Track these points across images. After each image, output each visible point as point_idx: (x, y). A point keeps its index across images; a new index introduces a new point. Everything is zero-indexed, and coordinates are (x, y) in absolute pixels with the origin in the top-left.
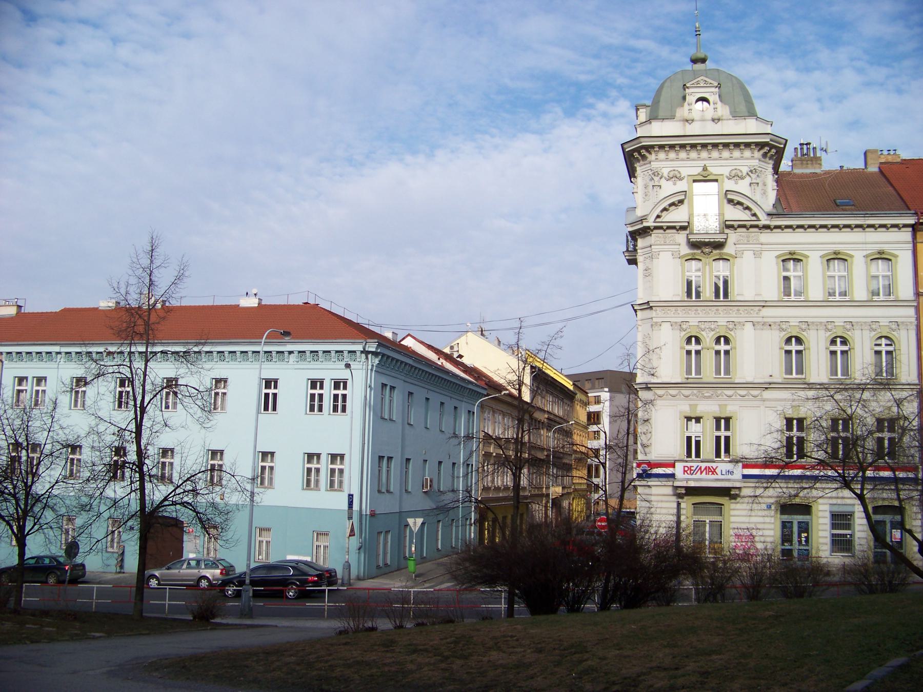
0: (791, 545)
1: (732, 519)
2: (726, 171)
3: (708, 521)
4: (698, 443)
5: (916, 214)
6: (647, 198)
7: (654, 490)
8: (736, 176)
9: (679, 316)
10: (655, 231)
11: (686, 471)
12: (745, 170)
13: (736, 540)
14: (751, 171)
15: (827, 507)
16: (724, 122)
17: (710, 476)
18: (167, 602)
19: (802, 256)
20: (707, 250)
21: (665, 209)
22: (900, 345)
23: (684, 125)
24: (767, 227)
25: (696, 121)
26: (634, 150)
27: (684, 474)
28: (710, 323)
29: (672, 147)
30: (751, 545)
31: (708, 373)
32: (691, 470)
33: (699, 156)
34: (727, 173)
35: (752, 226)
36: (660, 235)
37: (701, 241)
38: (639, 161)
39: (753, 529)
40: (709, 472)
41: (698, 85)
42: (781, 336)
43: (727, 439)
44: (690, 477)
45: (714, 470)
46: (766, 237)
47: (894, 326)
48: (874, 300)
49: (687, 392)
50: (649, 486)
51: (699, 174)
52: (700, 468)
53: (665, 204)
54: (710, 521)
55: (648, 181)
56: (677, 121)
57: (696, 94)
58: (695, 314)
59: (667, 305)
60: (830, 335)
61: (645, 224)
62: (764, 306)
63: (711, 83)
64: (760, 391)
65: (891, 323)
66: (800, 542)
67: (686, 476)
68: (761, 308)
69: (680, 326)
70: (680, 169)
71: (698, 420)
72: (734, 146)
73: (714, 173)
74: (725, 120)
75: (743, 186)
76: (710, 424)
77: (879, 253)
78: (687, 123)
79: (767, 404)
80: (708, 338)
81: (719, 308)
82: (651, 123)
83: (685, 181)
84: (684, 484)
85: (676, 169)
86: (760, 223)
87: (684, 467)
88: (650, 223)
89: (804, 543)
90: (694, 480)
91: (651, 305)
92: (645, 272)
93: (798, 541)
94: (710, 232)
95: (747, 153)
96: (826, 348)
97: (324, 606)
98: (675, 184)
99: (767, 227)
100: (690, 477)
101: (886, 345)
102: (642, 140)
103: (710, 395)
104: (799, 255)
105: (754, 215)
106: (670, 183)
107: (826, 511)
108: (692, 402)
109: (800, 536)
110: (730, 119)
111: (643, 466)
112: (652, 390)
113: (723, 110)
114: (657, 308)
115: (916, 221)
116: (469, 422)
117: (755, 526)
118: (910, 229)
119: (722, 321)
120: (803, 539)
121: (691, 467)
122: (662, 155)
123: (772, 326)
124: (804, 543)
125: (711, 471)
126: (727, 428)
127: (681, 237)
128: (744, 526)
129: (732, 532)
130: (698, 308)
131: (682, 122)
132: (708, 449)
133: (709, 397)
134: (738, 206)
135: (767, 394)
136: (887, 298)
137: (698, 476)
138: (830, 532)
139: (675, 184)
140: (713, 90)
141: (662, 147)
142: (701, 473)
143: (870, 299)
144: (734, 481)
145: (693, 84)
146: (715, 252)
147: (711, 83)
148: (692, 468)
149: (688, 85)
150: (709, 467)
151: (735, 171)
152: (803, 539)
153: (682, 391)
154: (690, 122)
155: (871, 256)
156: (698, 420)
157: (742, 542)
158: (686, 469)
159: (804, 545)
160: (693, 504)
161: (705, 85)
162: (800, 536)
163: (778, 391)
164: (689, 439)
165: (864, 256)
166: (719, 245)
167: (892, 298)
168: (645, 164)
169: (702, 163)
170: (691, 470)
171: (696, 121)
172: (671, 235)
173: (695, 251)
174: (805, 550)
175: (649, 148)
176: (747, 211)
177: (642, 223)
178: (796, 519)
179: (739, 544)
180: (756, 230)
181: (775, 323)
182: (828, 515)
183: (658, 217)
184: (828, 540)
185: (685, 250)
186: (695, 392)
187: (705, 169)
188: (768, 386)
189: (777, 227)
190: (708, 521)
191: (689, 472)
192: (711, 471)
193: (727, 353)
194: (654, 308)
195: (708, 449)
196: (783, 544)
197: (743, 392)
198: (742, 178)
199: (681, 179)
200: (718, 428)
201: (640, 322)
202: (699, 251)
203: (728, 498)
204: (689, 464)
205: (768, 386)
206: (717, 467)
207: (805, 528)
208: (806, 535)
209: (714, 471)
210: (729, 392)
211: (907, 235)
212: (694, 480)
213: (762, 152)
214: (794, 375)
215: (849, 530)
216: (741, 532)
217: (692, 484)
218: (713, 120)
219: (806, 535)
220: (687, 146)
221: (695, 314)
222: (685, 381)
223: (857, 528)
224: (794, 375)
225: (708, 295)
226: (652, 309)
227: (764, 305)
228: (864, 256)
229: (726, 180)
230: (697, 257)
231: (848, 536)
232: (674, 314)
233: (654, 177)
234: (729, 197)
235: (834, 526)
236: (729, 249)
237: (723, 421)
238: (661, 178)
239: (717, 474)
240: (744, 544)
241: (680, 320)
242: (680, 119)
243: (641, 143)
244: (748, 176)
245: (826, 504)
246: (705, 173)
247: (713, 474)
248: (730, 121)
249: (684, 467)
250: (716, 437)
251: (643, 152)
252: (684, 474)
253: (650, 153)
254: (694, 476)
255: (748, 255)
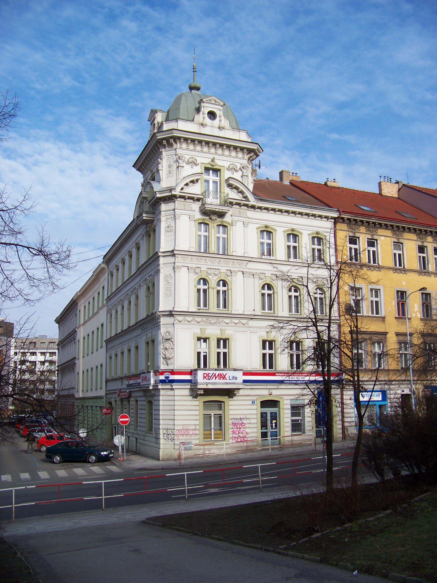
0: (267, 429)
1: (231, 412)
2: (226, 164)
3: (213, 414)
4: (205, 357)
5: (338, 211)
6: (170, 175)
7: (177, 392)
8: (233, 169)
9: (193, 263)
10: (178, 199)
11: (205, 377)
12: (239, 166)
13: (234, 427)
14: (243, 167)
15: (288, 402)
16: (226, 131)
17: (222, 381)
18: (187, 488)
19: (272, 229)
20: (214, 217)
21: (187, 185)
22: (231, 286)
23: (200, 128)
24: (253, 207)
25: (226, 129)
26: (163, 139)
27: (204, 379)
28: (214, 270)
29: (193, 141)
30: (243, 430)
31: (213, 307)
32: (208, 376)
33: (209, 151)
34: (227, 166)
35: (244, 205)
36: (181, 203)
37: (213, 210)
38: (164, 147)
39: (244, 419)
40: (221, 377)
41: (210, 102)
42: (260, 283)
43: (225, 354)
44: (208, 381)
45: (225, 376)
46: (251, 213)
47: (229, 273)
48: (263, 258)
49: (199, 319)
50: (172, 389)
51: (209, 163)
52: (215, 375)
53: (188, 181)
54: (214, 414)
55: (172, 162)
56: (195, 124)
57: (208, 108)
58: (204, 262)
59: (187, 254)
60: (262, 283)
61: (173, 193)
62: (250, 261)
63: (219, 103)
64: (247, 321)
65: (208, 269)
66: (272, 426)
67: (206, 381)
68: (248, 262)
69: (195, 270)
70: (196, 158)
71: (205, 340)
72: (191, 141)
73: (219, 164)
74: (226, 129)
75: (238, 175)
76: (214, 343)
77: (292, 230)
78: (201, 127)
79: (252, 330)
80: (213, 281)
81: (221, 259)
82: (177, 121)
83: (199, 166)
84: (205, 387)
85: (194, 157)
86: (250, 203)
87: (204, 374)
88: (177, 192)
89: (274, 427)
90: (212, 384)
91: (175, 253)
92: (167, 228)
93: (271, 426)
94: (213, 203)
95: (240, 155)
96: (259, 291)
97: (187, 487)
98: (192, 168)
99: (253, 207)
100: (208, 381)
101: (320, 294)
102: (174, 131)
103: (214, 322)
104: (271, 229)
105: (246, 197)
106: (189, 166)
107: (288, 404)
108: (202, 327)
109: (271, 423)
110: (230, 130)
111: (166, 373)
112: (174, 316)
113: (225, 123)
114: (179, 256)
115: (338, 216)
116: (114, 339)
117: (246, 416)
118: (333, 221)
119: (223, 269)
120: (274, 424)
121: (208, 374)
122: (184, 146)
123: (255, 276)
124: (274, 427)
125: (222, 377)
126: (271, 348)
127: (196, 206)
128: (238, 417)
129: (230, 422)
130: (207, 258)
131: (198, 125)
132: (213, 362)
133: (214, 323)
134: (234, 190)
135: (252, 323)
136: (295, 260)
137: (213, 380)
138: (291, 418)
139: (192, 168)
140: (219, 107)
141: (186, 139)
142: (216, 378)
143: (287, 260)
144: (238, 384)
145: (207, 100)
146: (218, 220)
147: (219, 103)
148: (209, 375)
149: (204, 100)
150: (221, 374)
151: (233, 165)
152: (274, 424)
153: (196, 318)
154: (221, 129)
155: (288, 231)
156: (205, 340)
157: (237, 428)
158: (205, 375)
159: (274, 429)
160: (204, 402)
161: (215, 103)
162: (271, 423)
163: (258, 321)
164: (199, 354)
165: (308, 234)
166: (221, 215)
167: (272, 258)
168: (170, 150)
169: (212, 157)
170: (208, 376)
171: (208, 126)
172: (189, 203)
173: (205, 217)
174: (275, 432)
175: (177, 139)
176: (240, 194)
177: (171, 192)
178: (268, 410)
179: (235, 430)
180: (245, 208)
181: (256, 273)
182: (289, 407)
183: (182, 189)
184: (289, 424)
185: (198, 216)
186: (204, 319)
187: (213, 160)
188: (252, 318)
189: (260, 208)
190: (213, 414)
191: (207, 378)
192: (222, 377)
193: (224, 292)
194: (176, 255)
195: (213, 362)
196: (261, 429)
197: (236, 321)
198: (237, 171)
199: (196, 165)
200: (264, 348)
201: (162, 265)
202: (208, 218)
203: (227, 397)
204: (207, 372)
205: (252, 318)
206: (226, 374)
207: (274, 416)
208: (275, 421)
209: (224, 377)
210: (227, 320)
211: (329, 224)
212: (212, 384)
213: (249, 156)
214: (267, 311)
215: (300, 416)
216: (236, 421)
217: (210, 387)
218: (219, 128)
219: (275, 421)
220: (203, 142)
221: (204, 262)
222: (197, 311)
223: (306, 415)
224: (267, 311)
225: (213, 250)
226: (175, 256)
227: (250, 260)
228: (308, 234)
229: (226, 170)
230: (206, 222)
231: (300, 421)
232: (232, 265)
233: (179, 160)
234: (231, 182)
235: (293, 415)
236: (227, 219)
237: (222, 341)
238: (183, 162)
239: (226, 379)
240: (238, 430)
241: (195, 266)
242: (197, 122)
243: (173, 133)
244: (240, 171)
245: (288, 399)
246: (212, 163)
247: (223, 379)
248: (229, 131)
249: (204, 374)
250: (217, 352)
251: (172, 141)
252: (204, 379)
253: (176, 143)
254: (210, 381)
255: (240, 225)
